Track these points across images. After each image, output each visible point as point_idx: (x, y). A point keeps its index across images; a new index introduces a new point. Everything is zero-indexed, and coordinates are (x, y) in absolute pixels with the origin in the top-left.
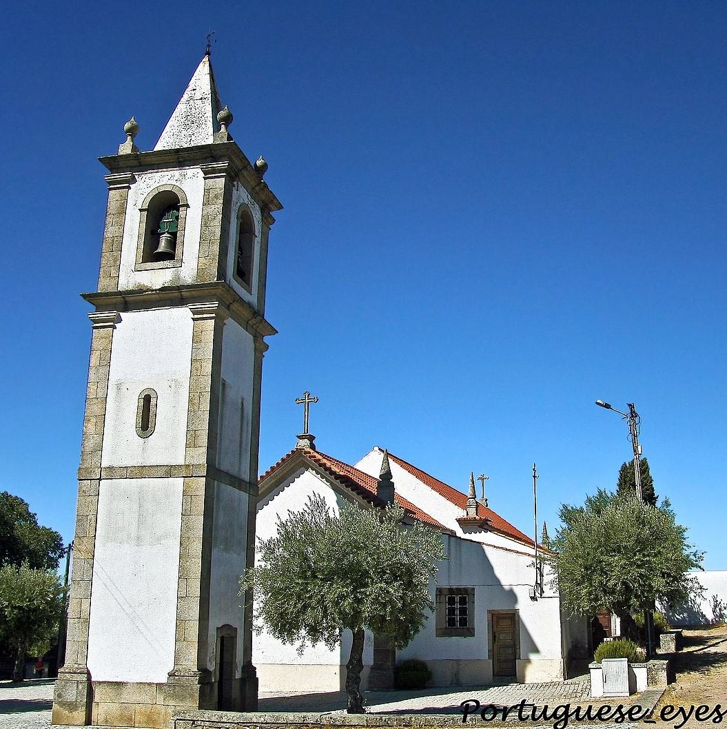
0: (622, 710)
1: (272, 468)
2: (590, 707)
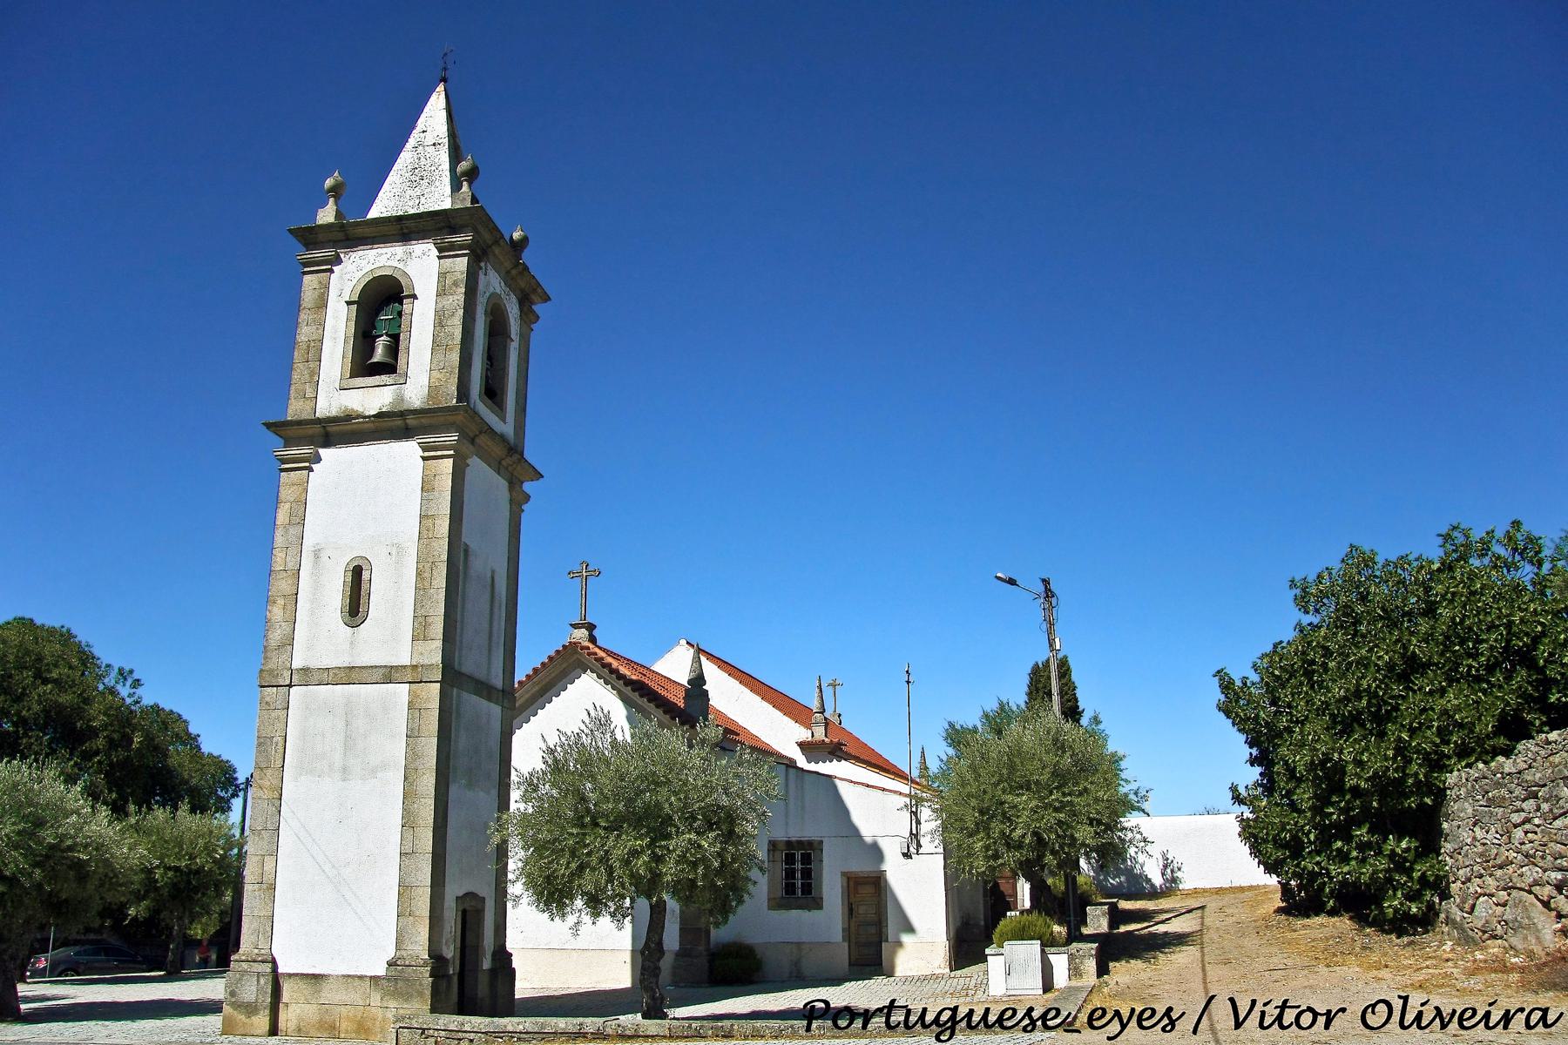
2: (987, 1010)
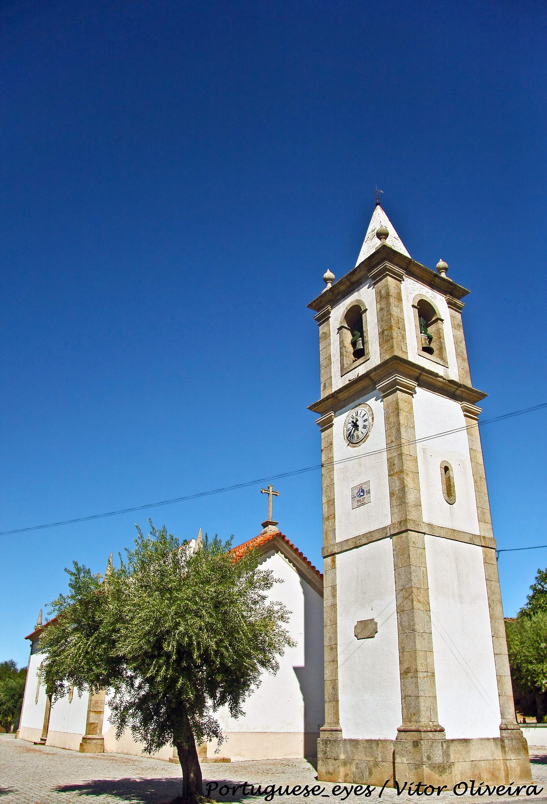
0: (370, 788)
1: (305, 559)
2: (288, 787)
